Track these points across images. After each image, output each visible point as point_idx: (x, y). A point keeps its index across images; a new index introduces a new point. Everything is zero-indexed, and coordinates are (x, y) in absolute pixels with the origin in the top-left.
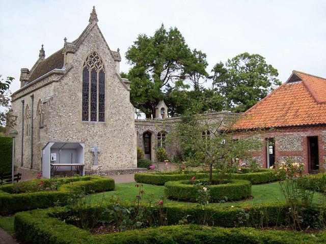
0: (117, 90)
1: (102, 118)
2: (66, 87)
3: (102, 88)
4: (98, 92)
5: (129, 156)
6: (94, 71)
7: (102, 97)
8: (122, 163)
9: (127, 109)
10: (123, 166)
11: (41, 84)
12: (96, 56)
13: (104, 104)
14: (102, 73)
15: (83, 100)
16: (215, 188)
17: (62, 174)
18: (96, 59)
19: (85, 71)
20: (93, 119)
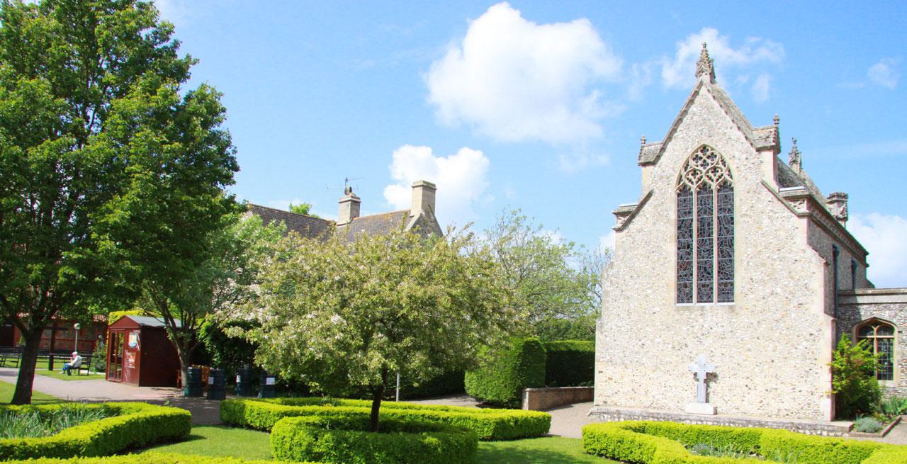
0: (766, 222)
1: (727, 293)
2: (639, 236)
3: (728, 223)
4: (715, 236)
5: (805, 388)
6: (704, 188)
7: (727, 245)
8: (781, 406)
9: (798, 266)
10: (783, 413)
11: (42, 360)
12: (700, 154)
13: (731, 261)
14: (726, 187)
15: (680, 257)
16: (577, 386)
17: (168, 312)
18: (700, 162)
19: (683, 191)
20: (705, 296)
